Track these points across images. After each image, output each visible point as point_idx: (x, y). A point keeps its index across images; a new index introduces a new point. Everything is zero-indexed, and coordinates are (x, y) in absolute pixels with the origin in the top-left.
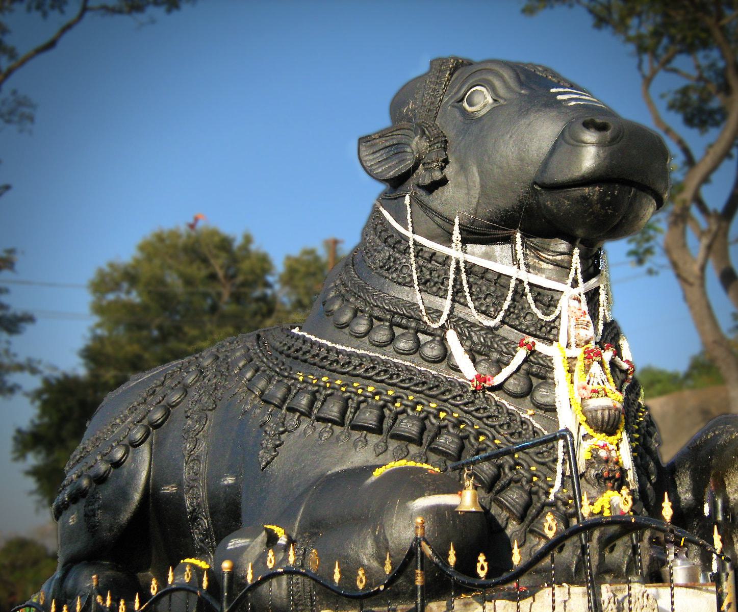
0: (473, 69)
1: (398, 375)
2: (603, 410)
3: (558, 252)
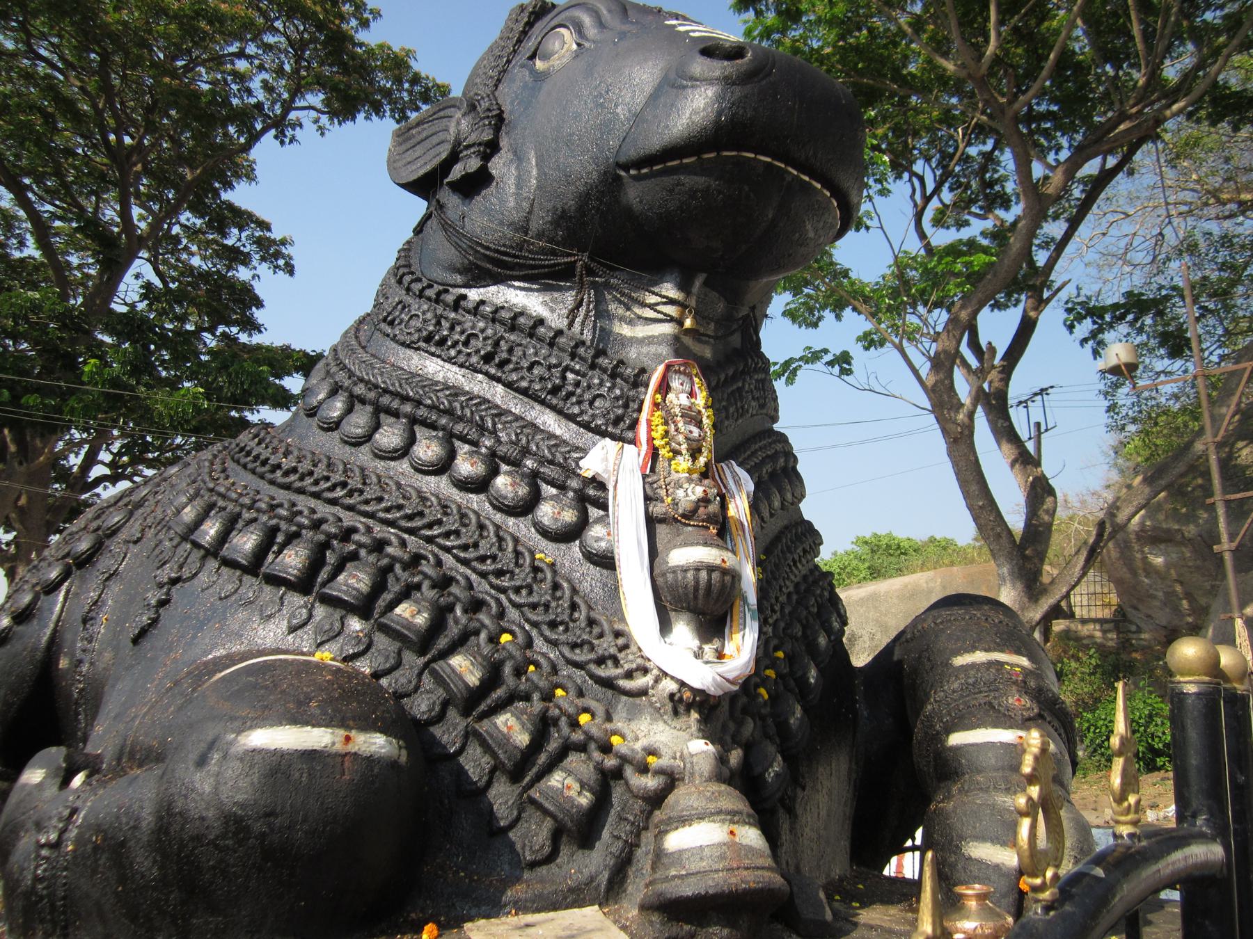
0: (556, 11)
1: (361, 492)
2: (697, 570)
3: (664, 297)
